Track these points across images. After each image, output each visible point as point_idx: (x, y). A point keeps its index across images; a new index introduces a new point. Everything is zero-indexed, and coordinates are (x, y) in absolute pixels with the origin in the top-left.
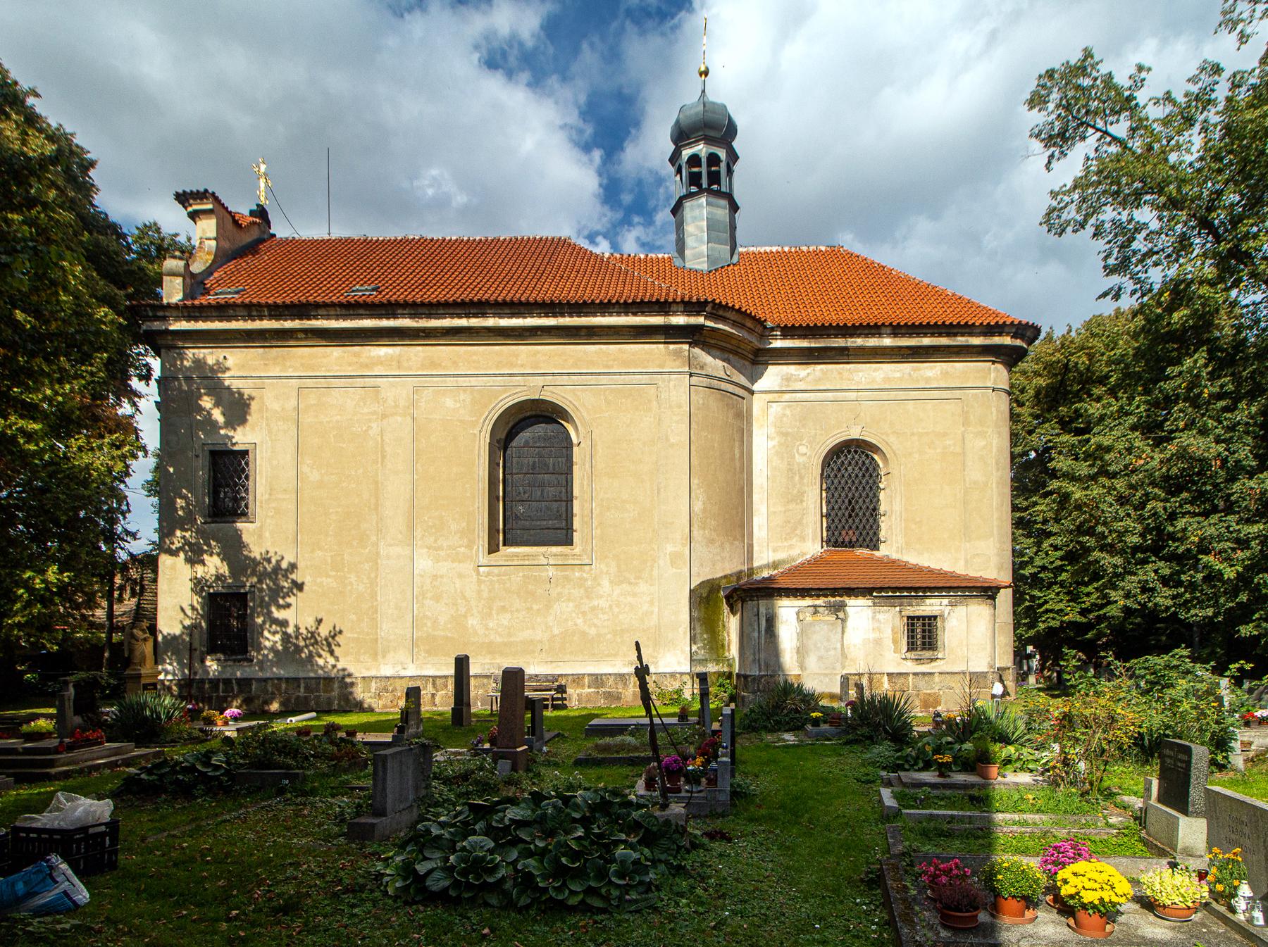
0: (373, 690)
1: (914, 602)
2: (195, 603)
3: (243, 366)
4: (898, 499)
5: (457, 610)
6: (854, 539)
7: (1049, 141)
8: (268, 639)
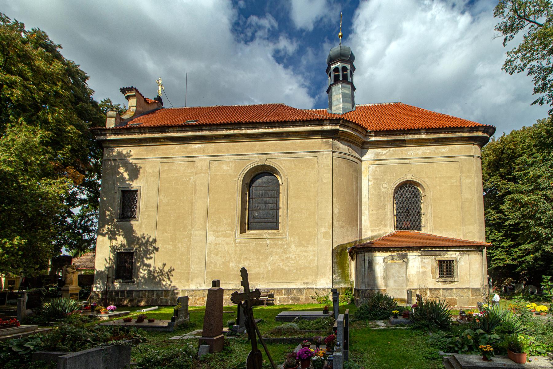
1: (442, 253)
2: (111, 257)
3: (137, 154)
4: (430, 207)
5: (225, 259)
6: (409, 226)
8: (141, 273)
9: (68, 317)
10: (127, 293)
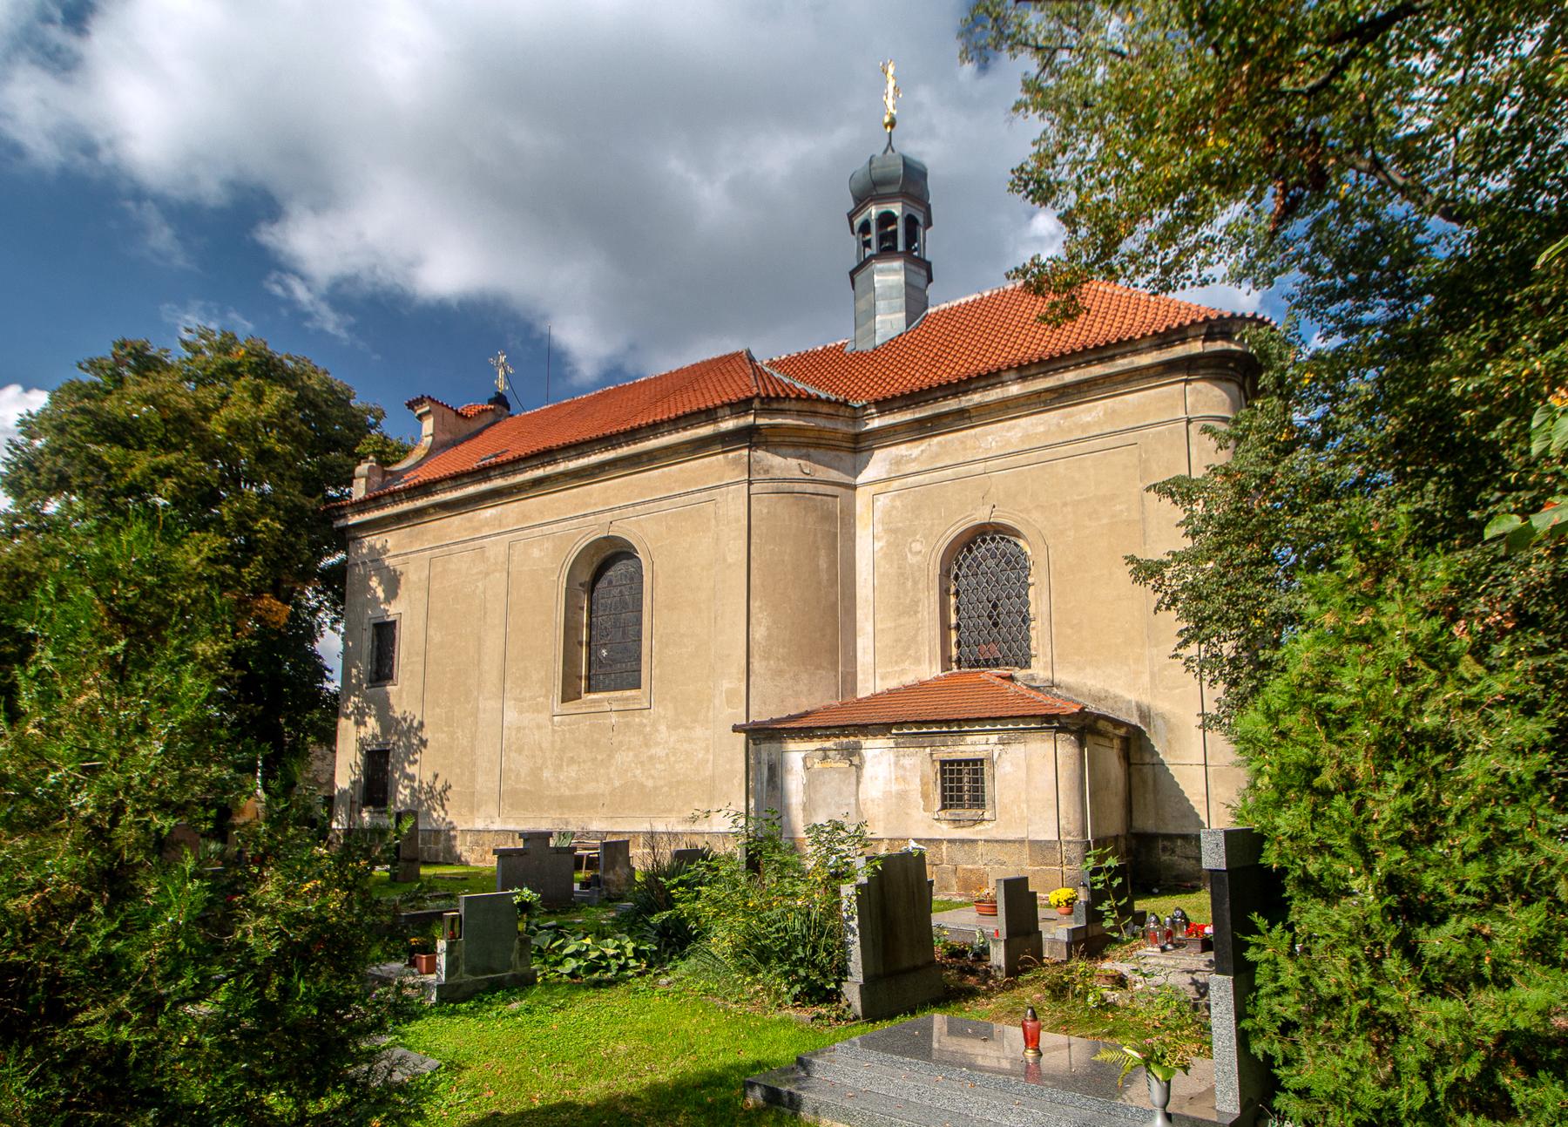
1: (950, 740)
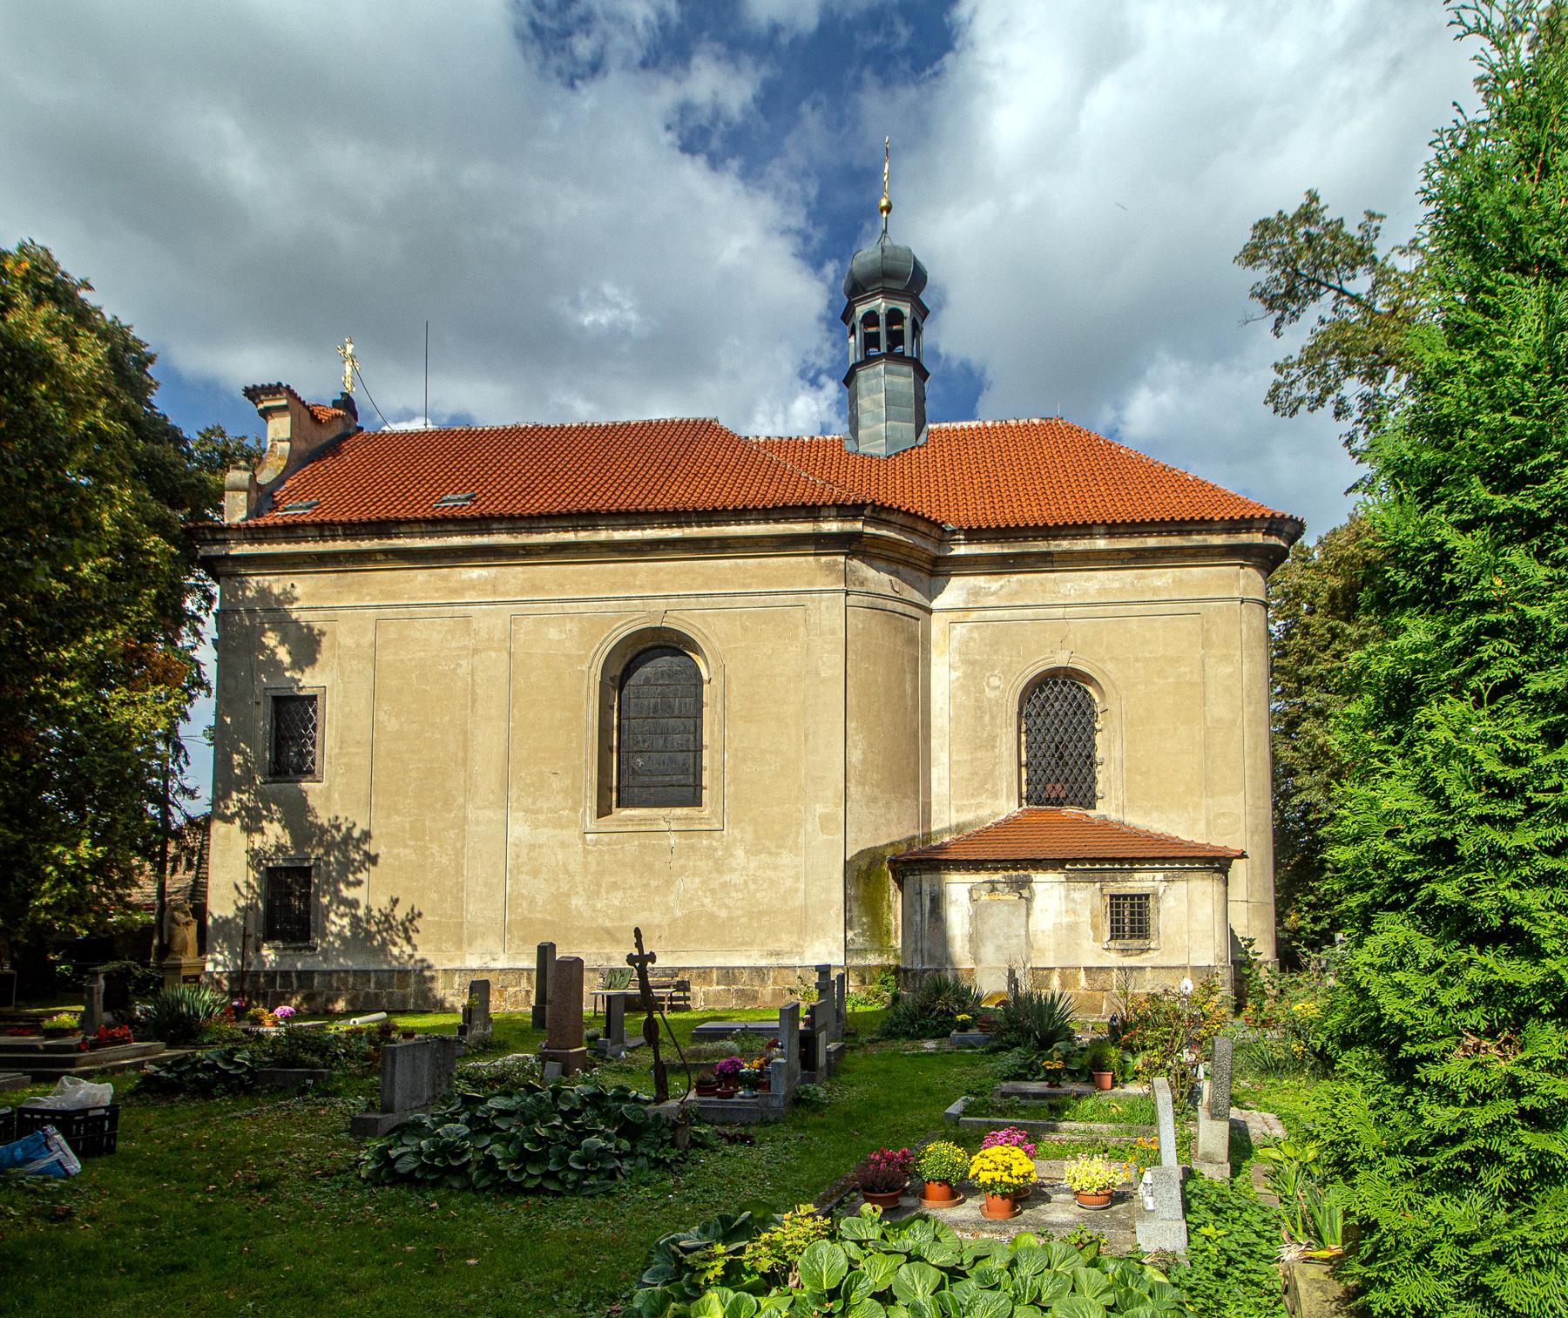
0: (456, 986)
1: (1119, 876)
2: (251, 880)
3: (313, 595)
5: (559, 887)
6: (1062, 795)
7: (1271, 303)
8: (334, 923)
9: (203, 1031)
10: (299, 978)
